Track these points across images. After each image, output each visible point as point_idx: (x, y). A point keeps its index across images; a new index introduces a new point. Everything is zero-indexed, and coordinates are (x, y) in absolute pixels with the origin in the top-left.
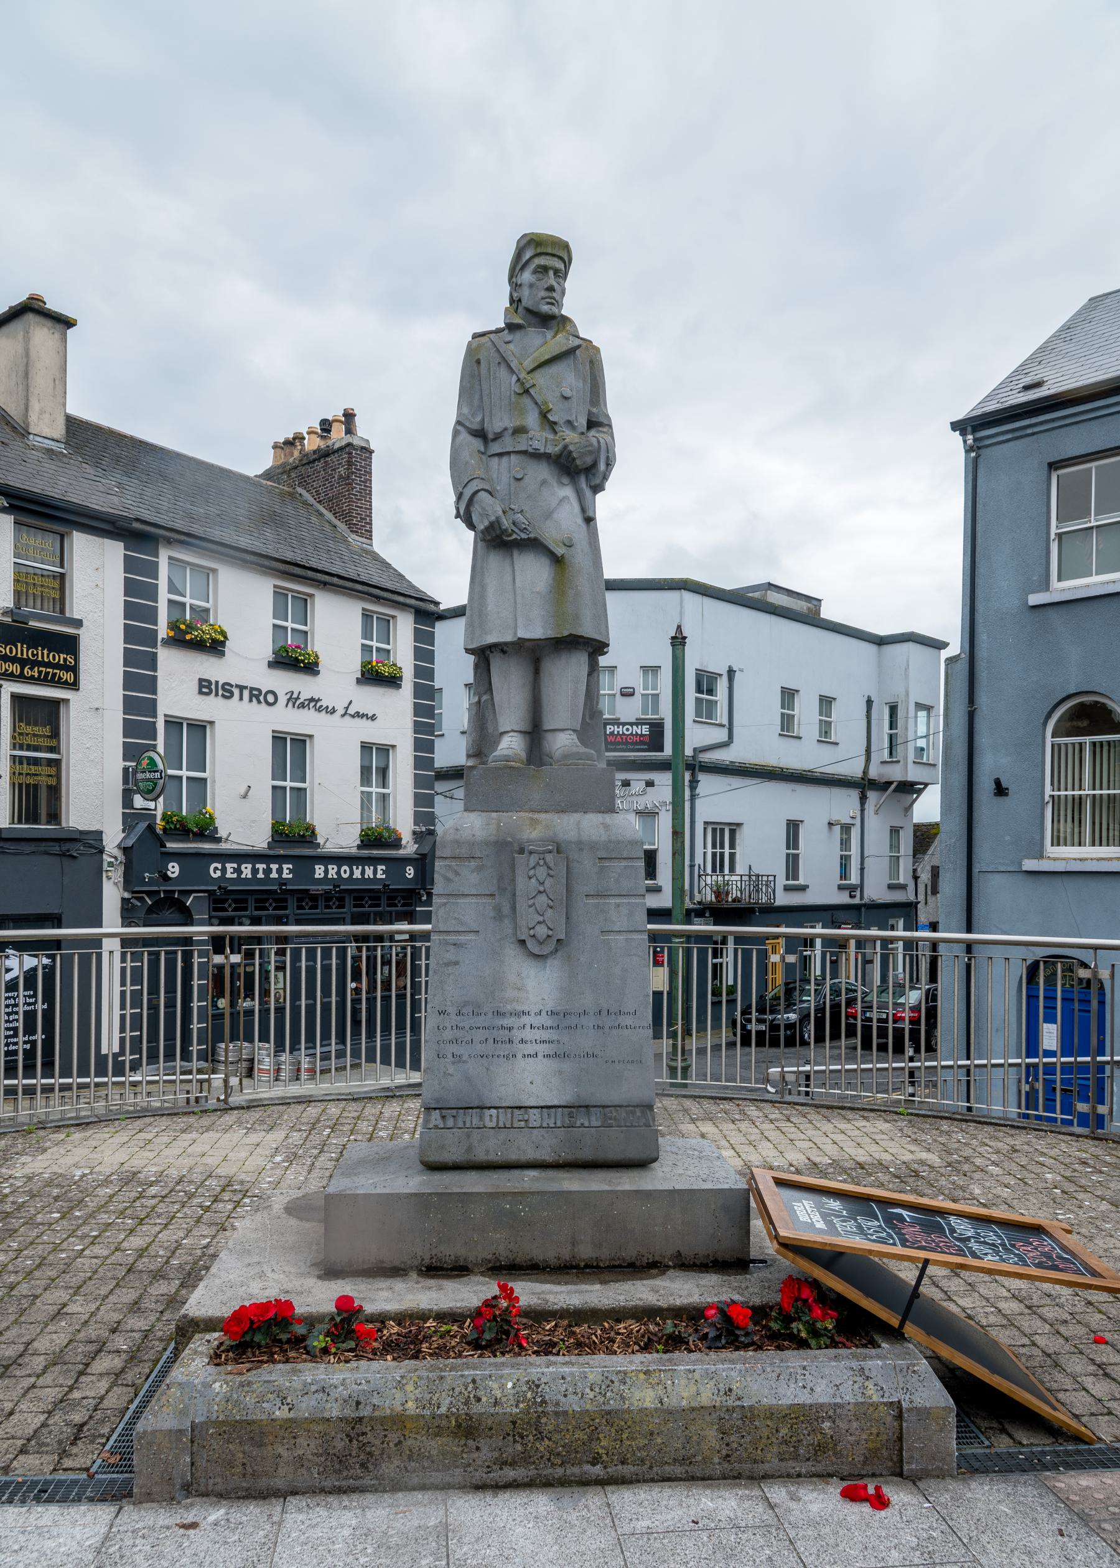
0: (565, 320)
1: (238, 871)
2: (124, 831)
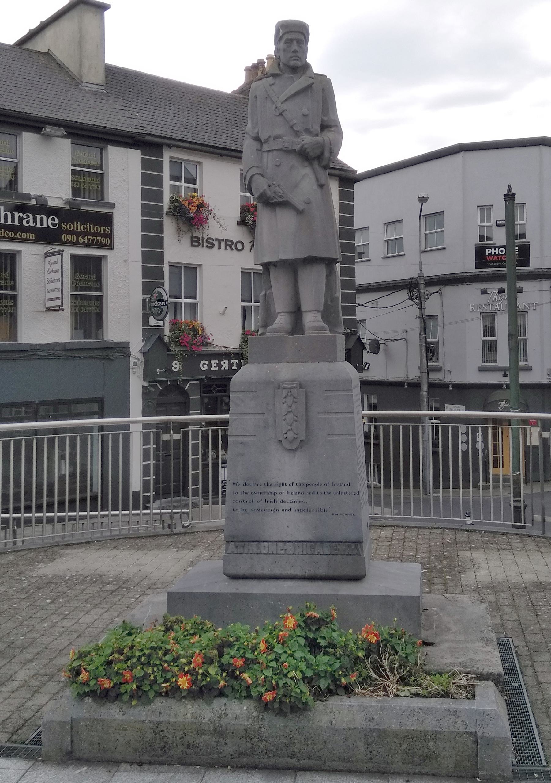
1: (219, 365)
2: (143, 341)
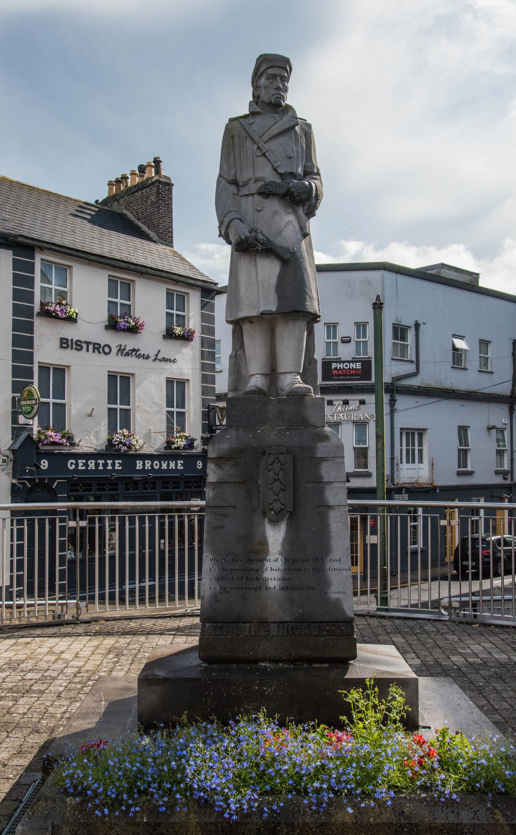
0: (289, 108)
1: (86, 465)
2: (12, 439)
